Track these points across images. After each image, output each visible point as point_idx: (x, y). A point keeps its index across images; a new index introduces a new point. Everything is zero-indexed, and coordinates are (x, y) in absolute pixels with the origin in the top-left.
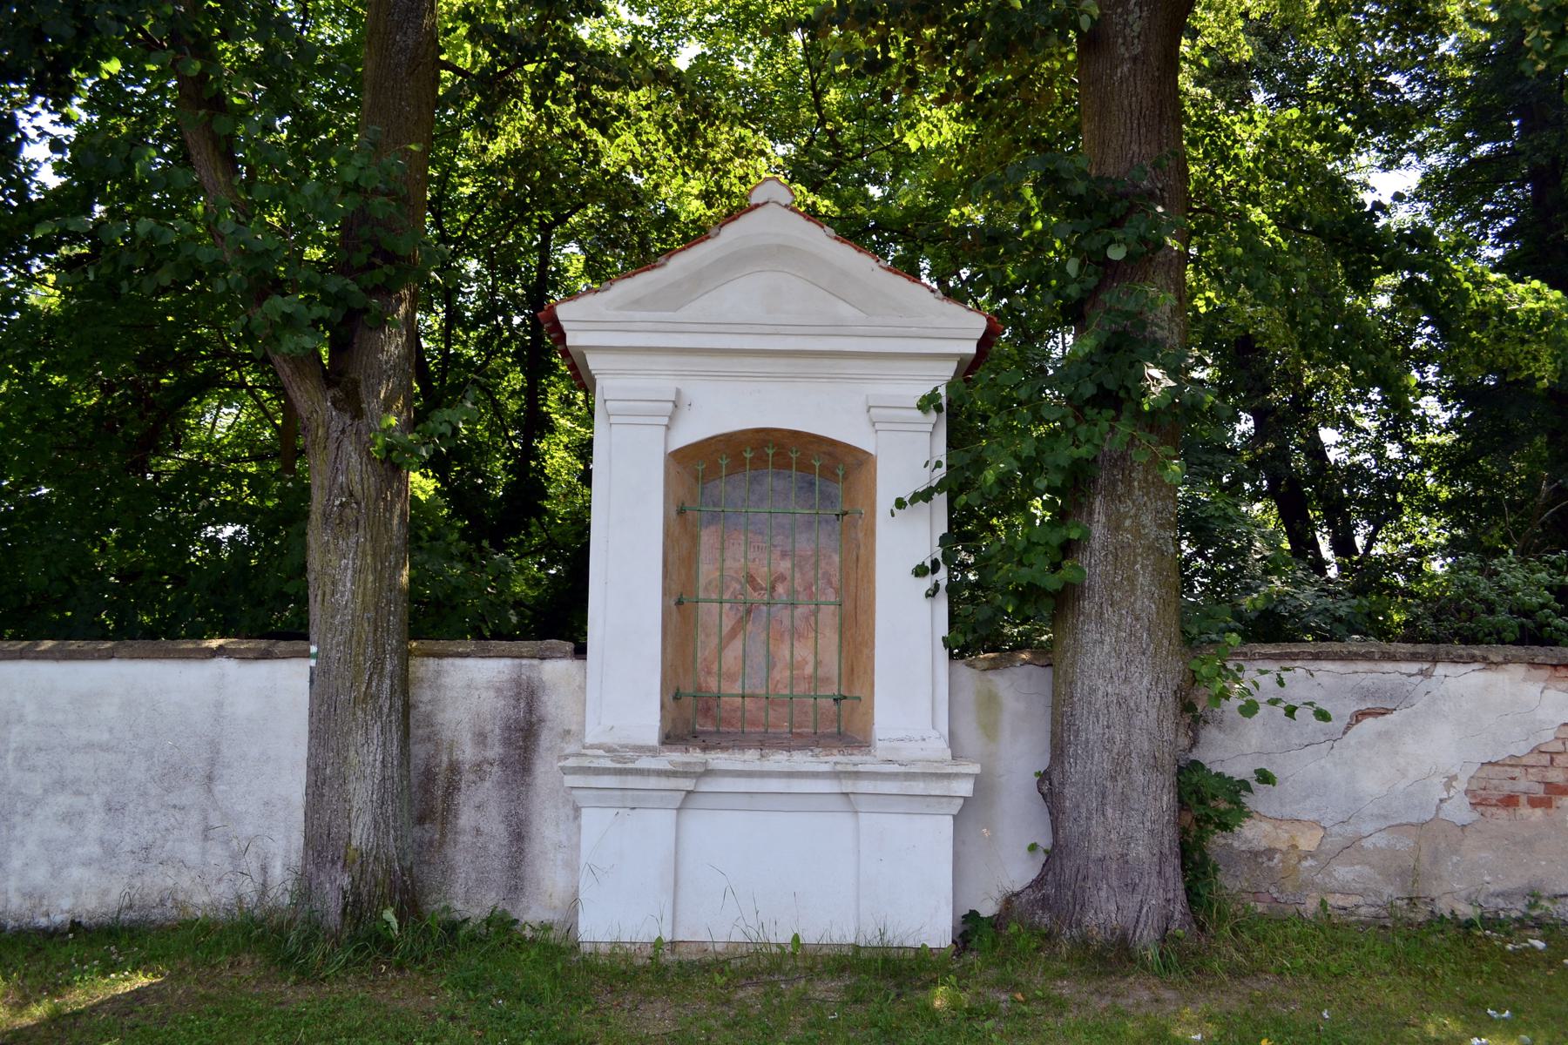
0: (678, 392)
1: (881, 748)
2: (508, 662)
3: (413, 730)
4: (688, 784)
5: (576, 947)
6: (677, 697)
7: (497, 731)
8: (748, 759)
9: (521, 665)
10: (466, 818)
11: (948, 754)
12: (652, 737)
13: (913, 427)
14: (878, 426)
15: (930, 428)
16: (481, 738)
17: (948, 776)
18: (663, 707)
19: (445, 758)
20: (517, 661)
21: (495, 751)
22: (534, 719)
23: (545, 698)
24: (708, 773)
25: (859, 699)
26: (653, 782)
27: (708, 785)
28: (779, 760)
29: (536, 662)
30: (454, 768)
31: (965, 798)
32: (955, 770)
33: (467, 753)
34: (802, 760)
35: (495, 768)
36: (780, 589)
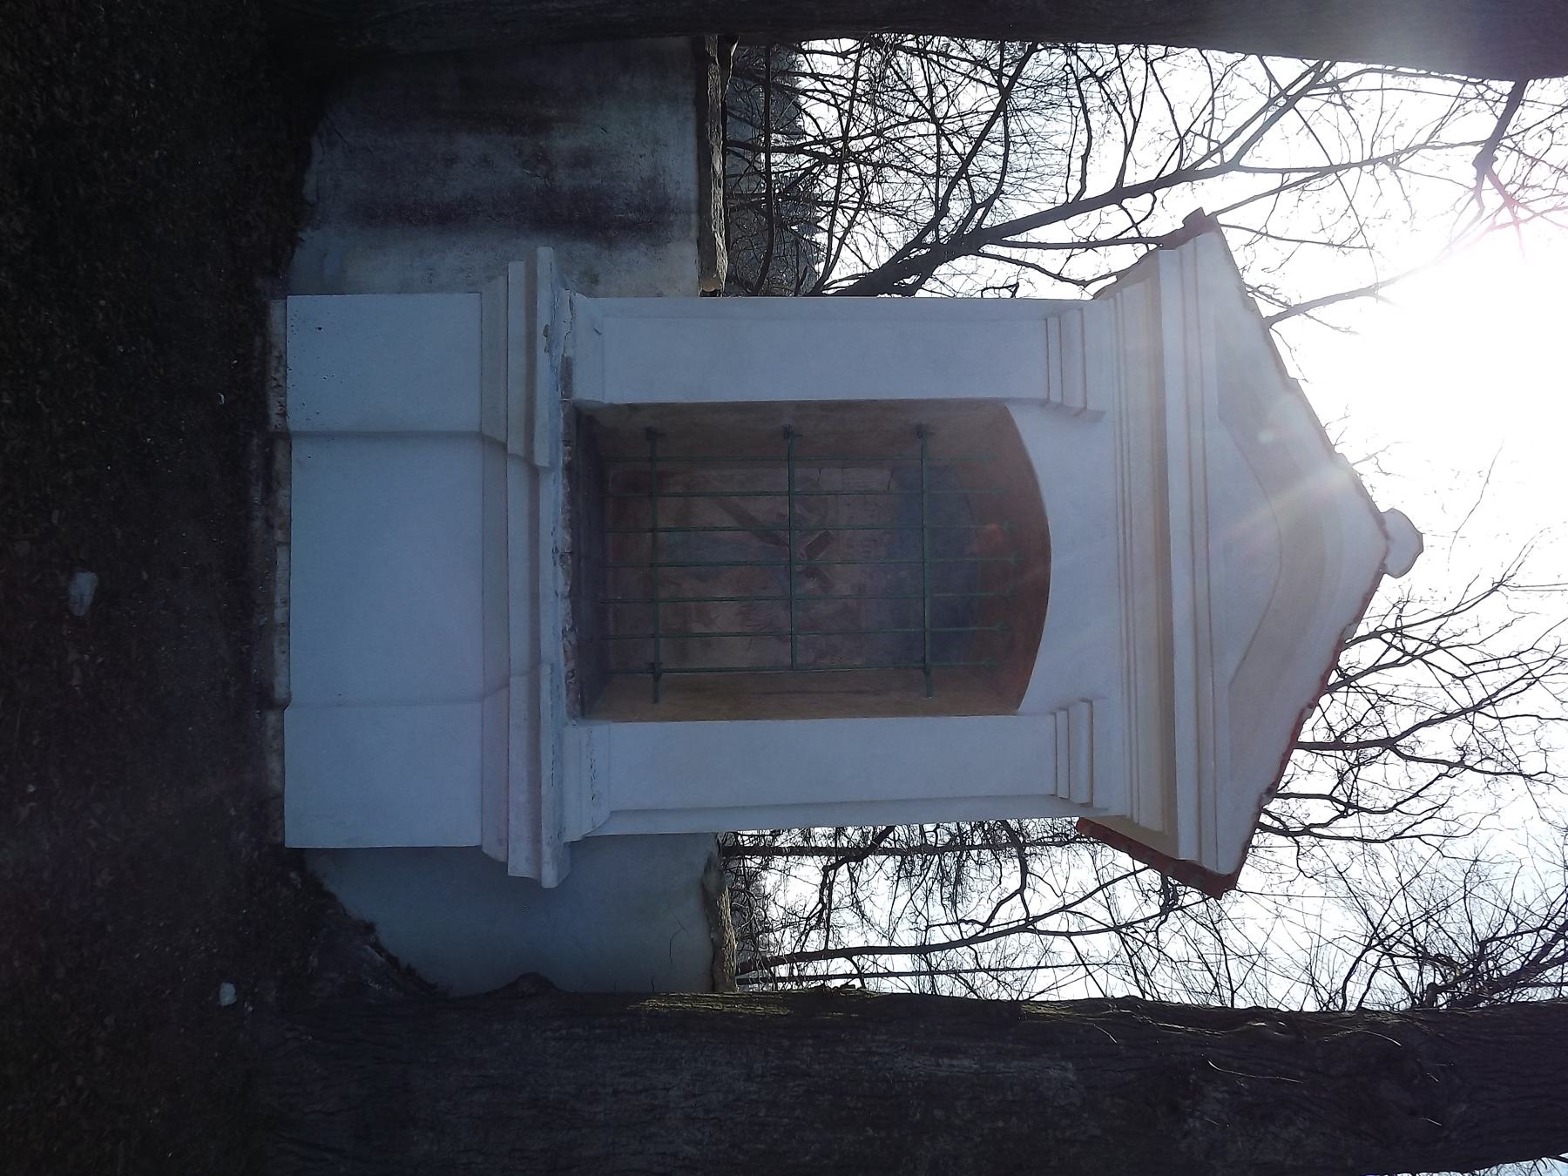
0: (1098, 416)
1: (577, 733)
2: (693, 195)
3: (1345, 162)
4: (516, 445)
5: (285, 291)
6: (651, 434)
7: (595, 182)
8: (554, 532)
9: (688, 213)
10: (469, 145)
11: (573, 835)
12: (587, 391)
13: (1062, 772)
14: (1061, 715)
15: (1062, 793)
16: (583, 159)
17: (536, 839)
18: (633, 408)
19: (554, 112)
20: (694, 207)
21: (565, 180)
22: (611, 233)
23: (643, 247)
24: (534, 473)
25: (656, 701)
26: (517, 391)
27: (517, 479)
28: (555, 580)
29: (694, 234)
30: (541, 126)
31: (505, 864)
32: (547, 851)
33: (563, 142)
34: (556, 615)
35: (541, 182)
36: (811, 585)
